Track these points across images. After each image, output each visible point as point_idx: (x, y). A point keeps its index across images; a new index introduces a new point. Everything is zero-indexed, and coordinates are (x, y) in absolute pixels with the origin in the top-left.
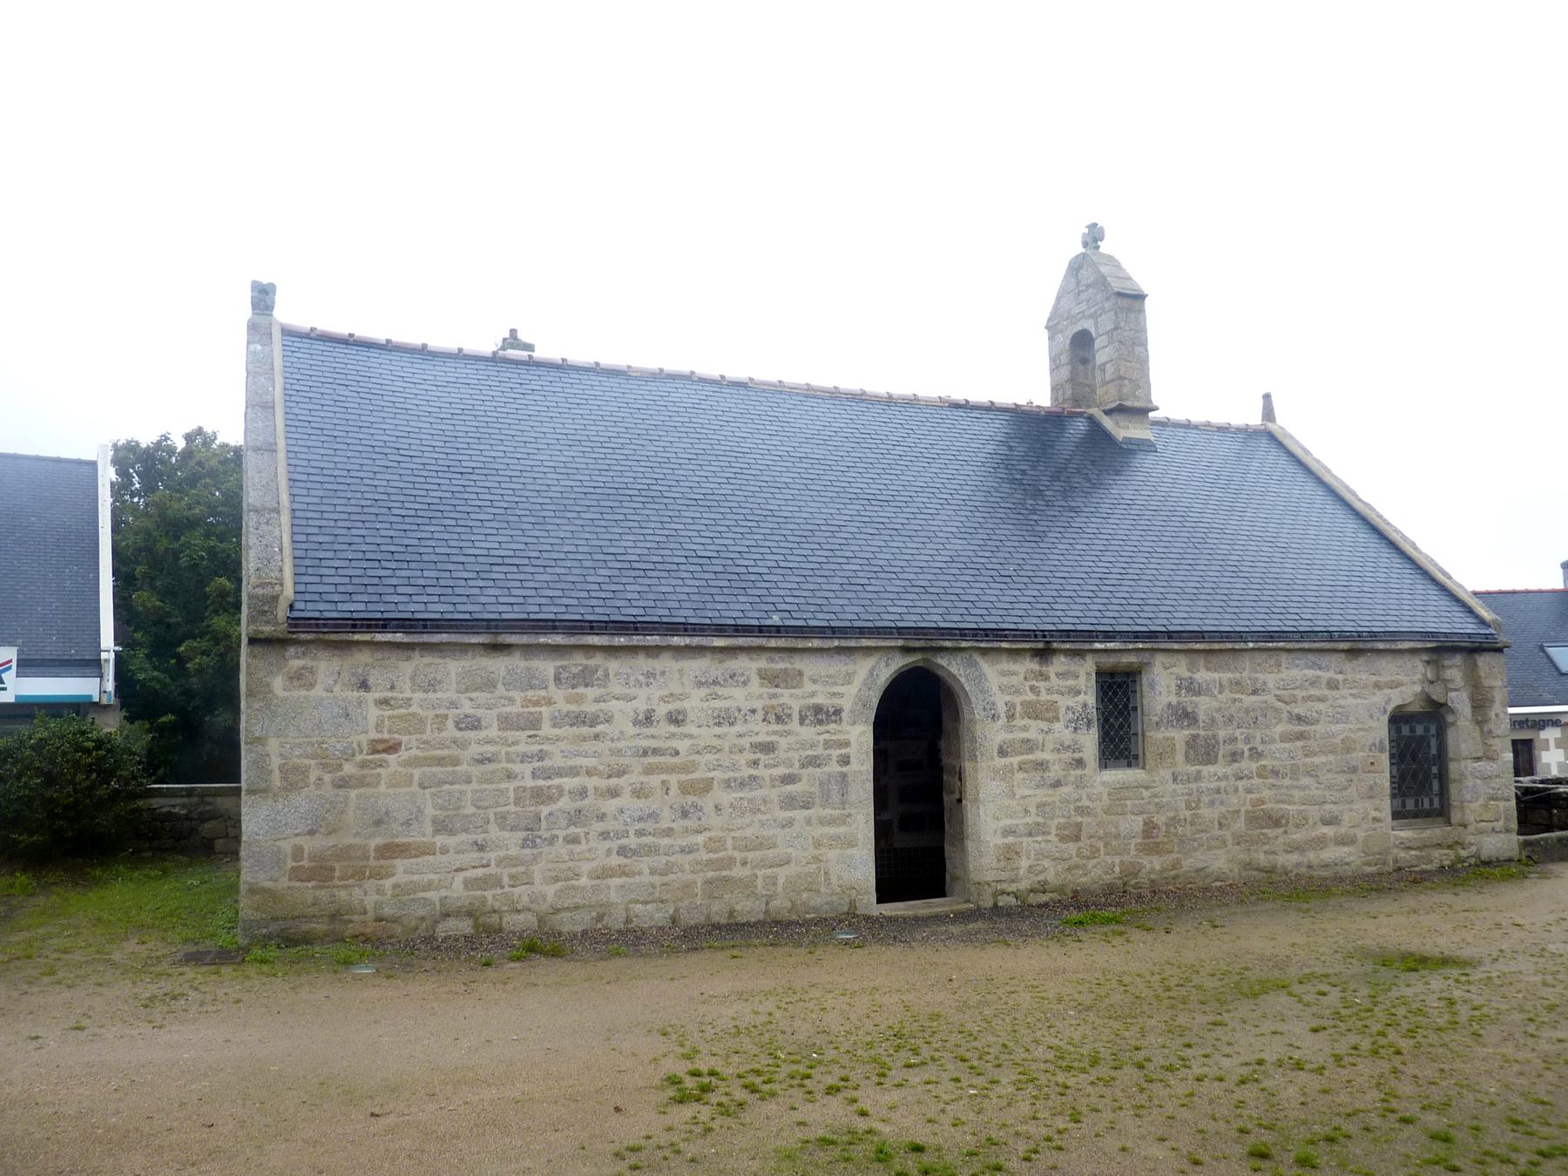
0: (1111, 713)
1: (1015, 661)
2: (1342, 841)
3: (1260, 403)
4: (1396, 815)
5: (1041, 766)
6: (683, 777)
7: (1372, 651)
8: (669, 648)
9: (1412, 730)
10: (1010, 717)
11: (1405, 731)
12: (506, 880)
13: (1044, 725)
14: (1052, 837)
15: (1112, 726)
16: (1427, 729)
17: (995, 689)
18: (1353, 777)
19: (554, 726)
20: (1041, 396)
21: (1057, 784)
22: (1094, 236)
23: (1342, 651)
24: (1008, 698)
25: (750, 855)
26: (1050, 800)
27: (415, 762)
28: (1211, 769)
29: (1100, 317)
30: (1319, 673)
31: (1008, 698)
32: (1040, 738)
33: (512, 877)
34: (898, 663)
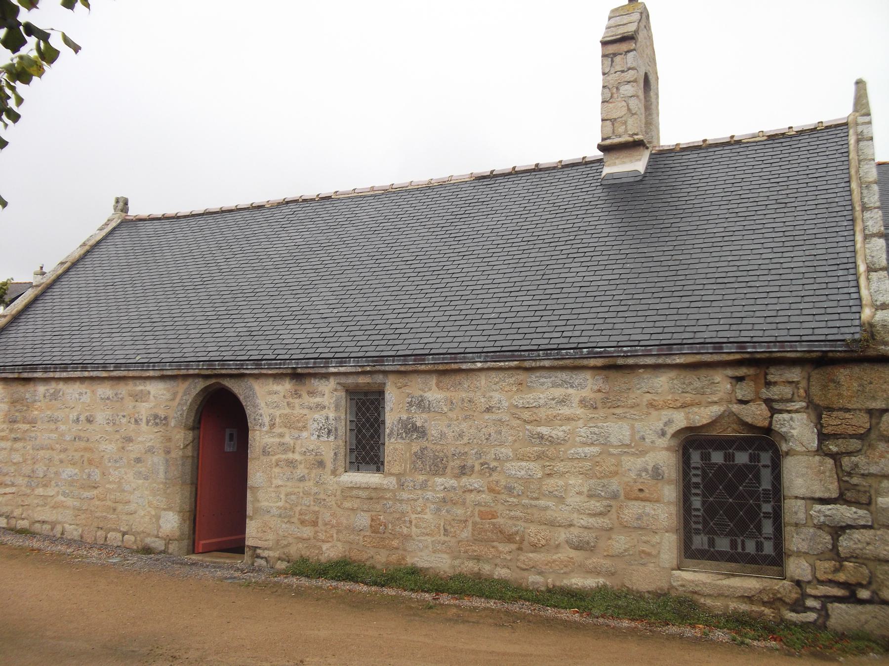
0: (364, 425)
1: (278, 384)
3: (851, 90)
5: (291, 464)
7: (460, 371)
8: (53, 379)
9: (729, 457)
10: (272, 426)
13: (296, 433)
15: (364, 436)
16: (754, 458)
17: (263, 405)
18: (612, 503)
21: (302, 479)
23: (595, 368)
24: (271, 411)
26: (296, 490)
28: (439, 480)
30: (571, 391)
31: (271, 411)
32: (292, 442)
34: (201, 385)
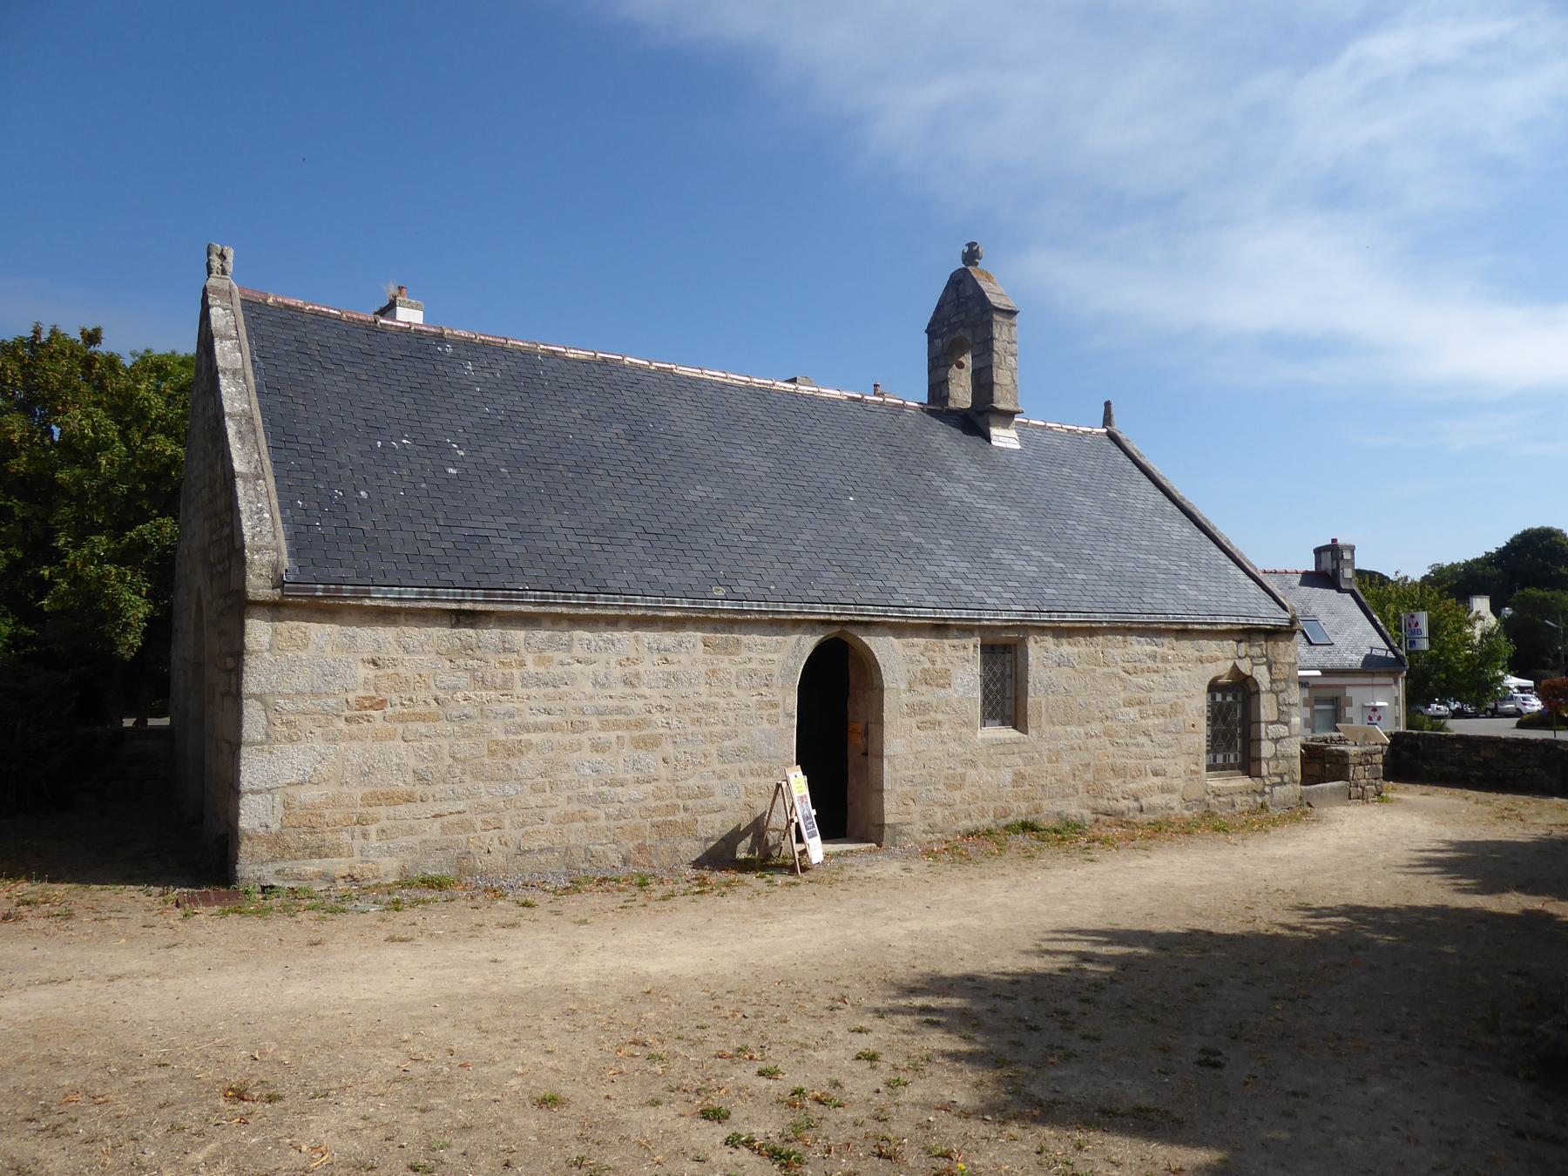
2: (1164, 790)
4: (1210, 768)
6: (636, 733)
9: (1224, 698)
11: (1219, 697)
12: (479, 825)
14: (941, 786)
19: (525, 686)
20: (1312, 568)
22: (971, 256)
25: (690, 803)
27: (401, 718)
29: (1334, 540)
33: (484, 822)
